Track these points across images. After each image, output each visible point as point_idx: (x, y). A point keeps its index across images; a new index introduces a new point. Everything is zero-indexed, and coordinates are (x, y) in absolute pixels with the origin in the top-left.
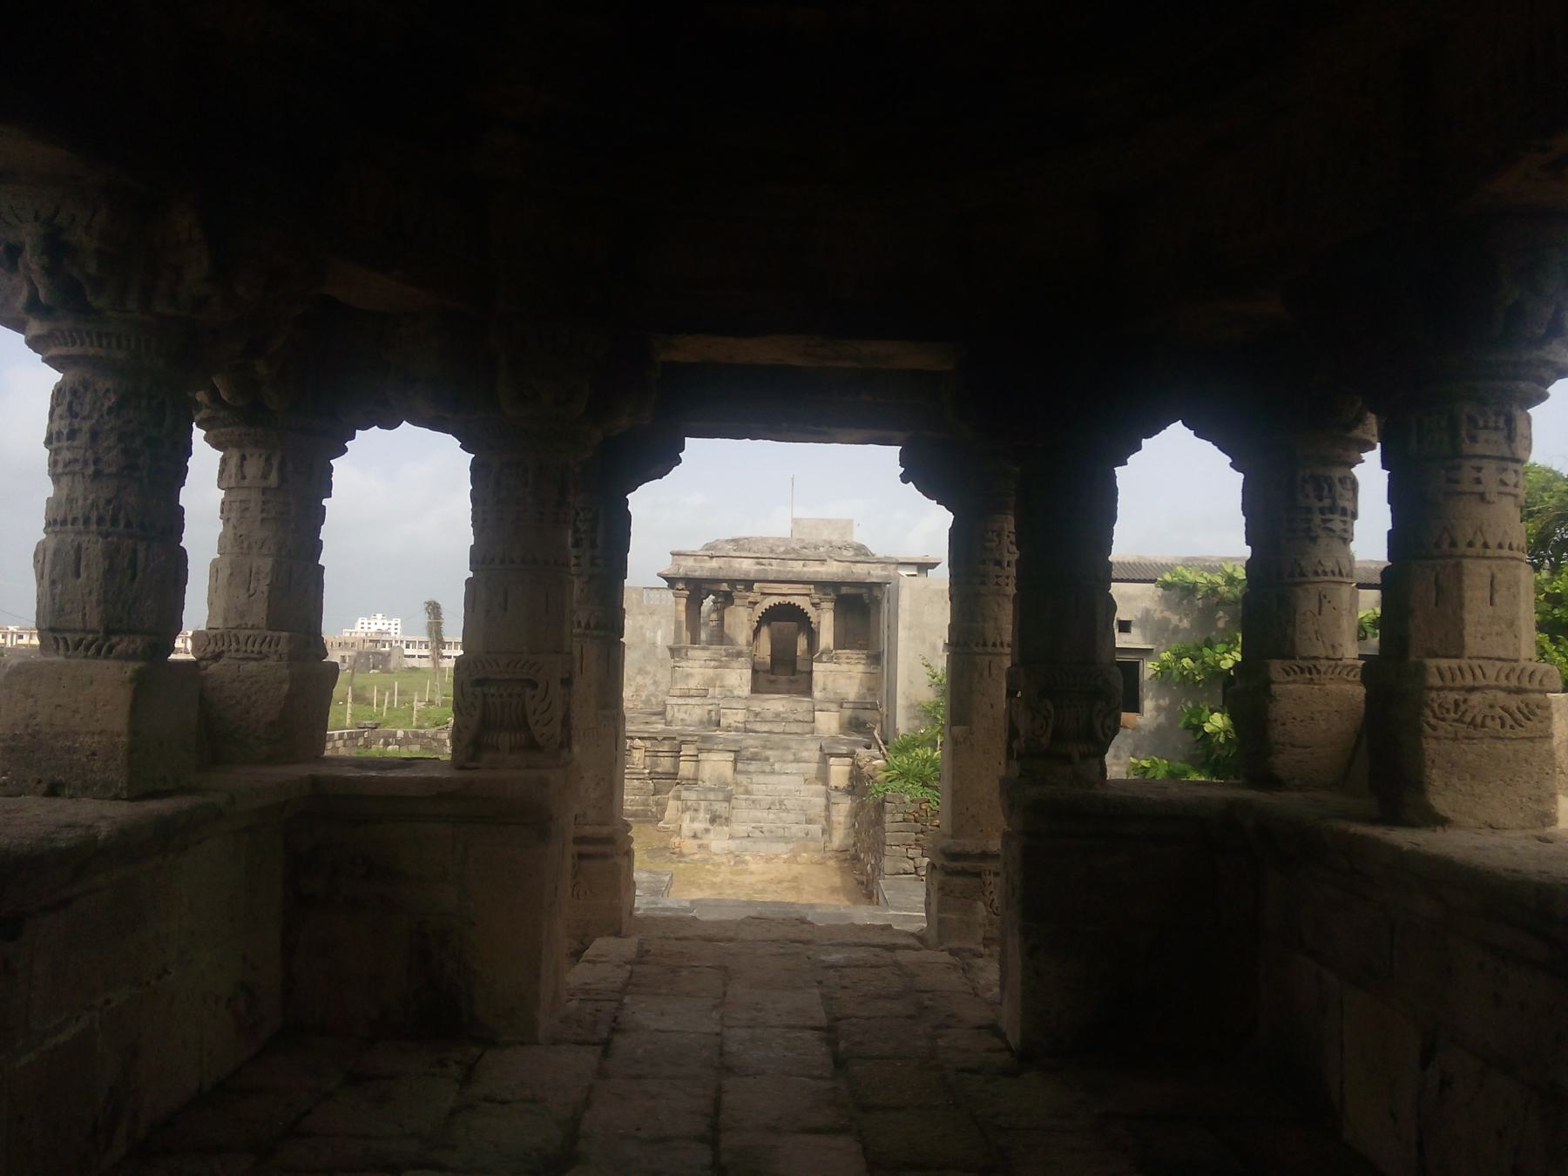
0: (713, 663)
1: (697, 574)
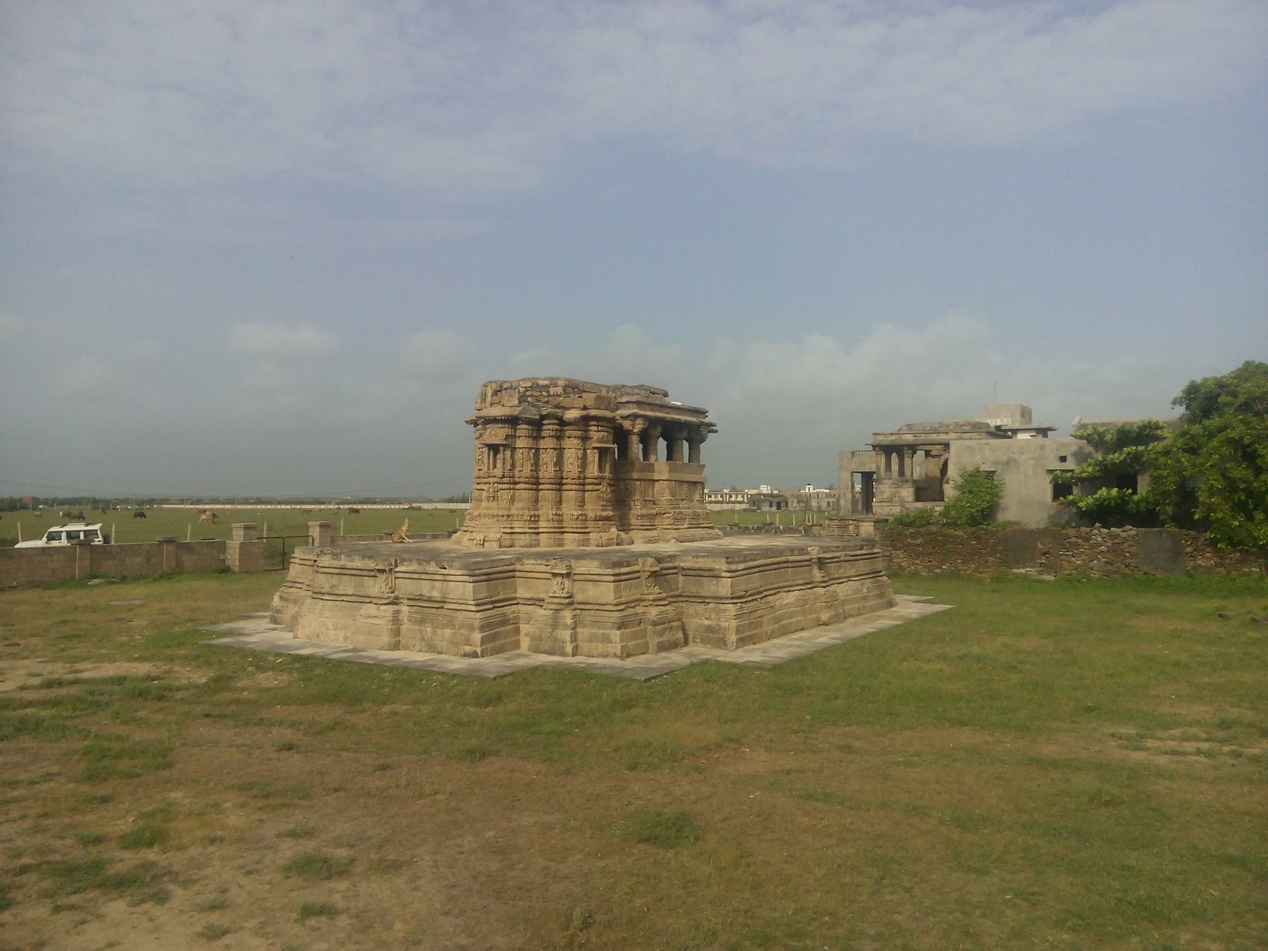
0: (894, 486)
1: (884, 443)
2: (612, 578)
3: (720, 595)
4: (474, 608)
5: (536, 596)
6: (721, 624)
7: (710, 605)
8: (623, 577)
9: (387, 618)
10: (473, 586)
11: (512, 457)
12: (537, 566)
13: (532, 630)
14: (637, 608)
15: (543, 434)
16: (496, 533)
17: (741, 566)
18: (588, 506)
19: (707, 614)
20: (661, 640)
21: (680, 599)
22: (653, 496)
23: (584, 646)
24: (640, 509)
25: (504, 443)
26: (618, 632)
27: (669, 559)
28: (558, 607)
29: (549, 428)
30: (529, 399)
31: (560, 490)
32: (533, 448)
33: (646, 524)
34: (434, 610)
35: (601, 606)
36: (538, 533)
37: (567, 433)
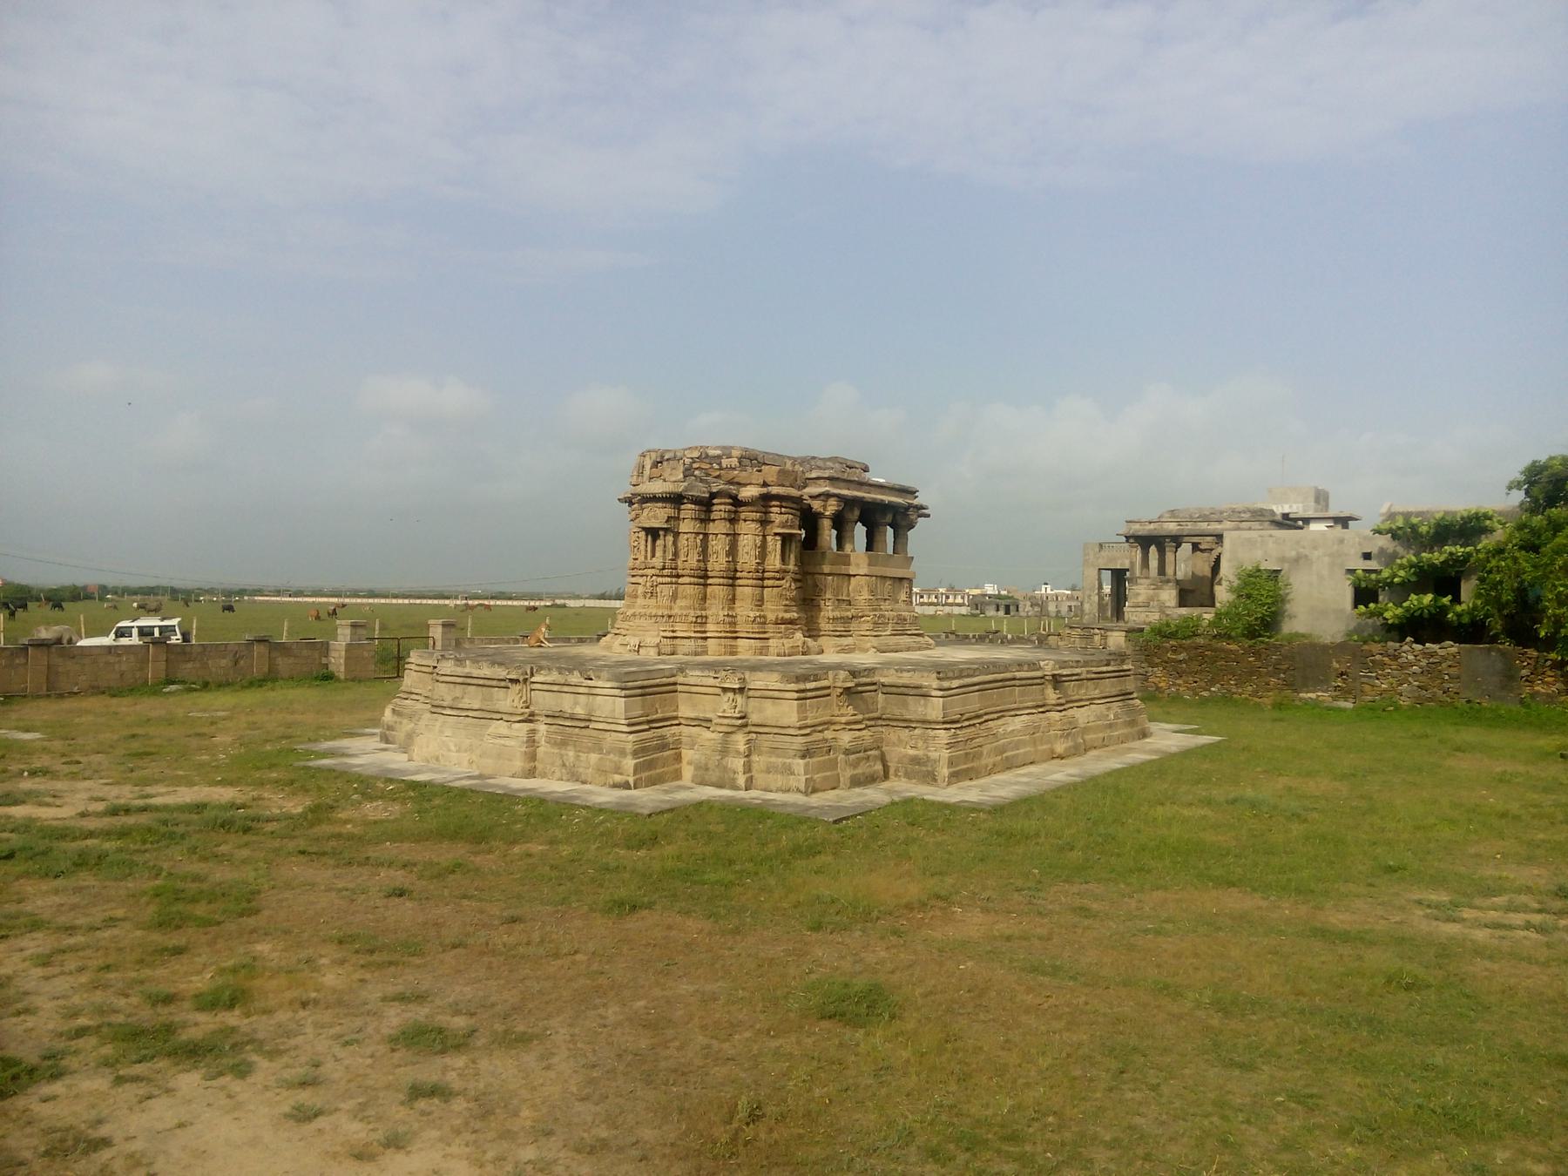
1: (1140, 533)
2: (796, 695)
3: (929, 718)
5: (701, 715)
6: (930, 754)
7: (916, 731)
8: (809, 694)
11: (675, 543)
12: (703, 679)
13: (697, 757)
17: (956, 683)
18: (768, 605)
21: (880, 722)
22: (848, 595)
23: (760, 778)
26: (802, 762)
28: (730, 729)
29: (720, 508)
30: (697, 472)
34: (577, 730)
36: (706, 638)
37: (743, 516)
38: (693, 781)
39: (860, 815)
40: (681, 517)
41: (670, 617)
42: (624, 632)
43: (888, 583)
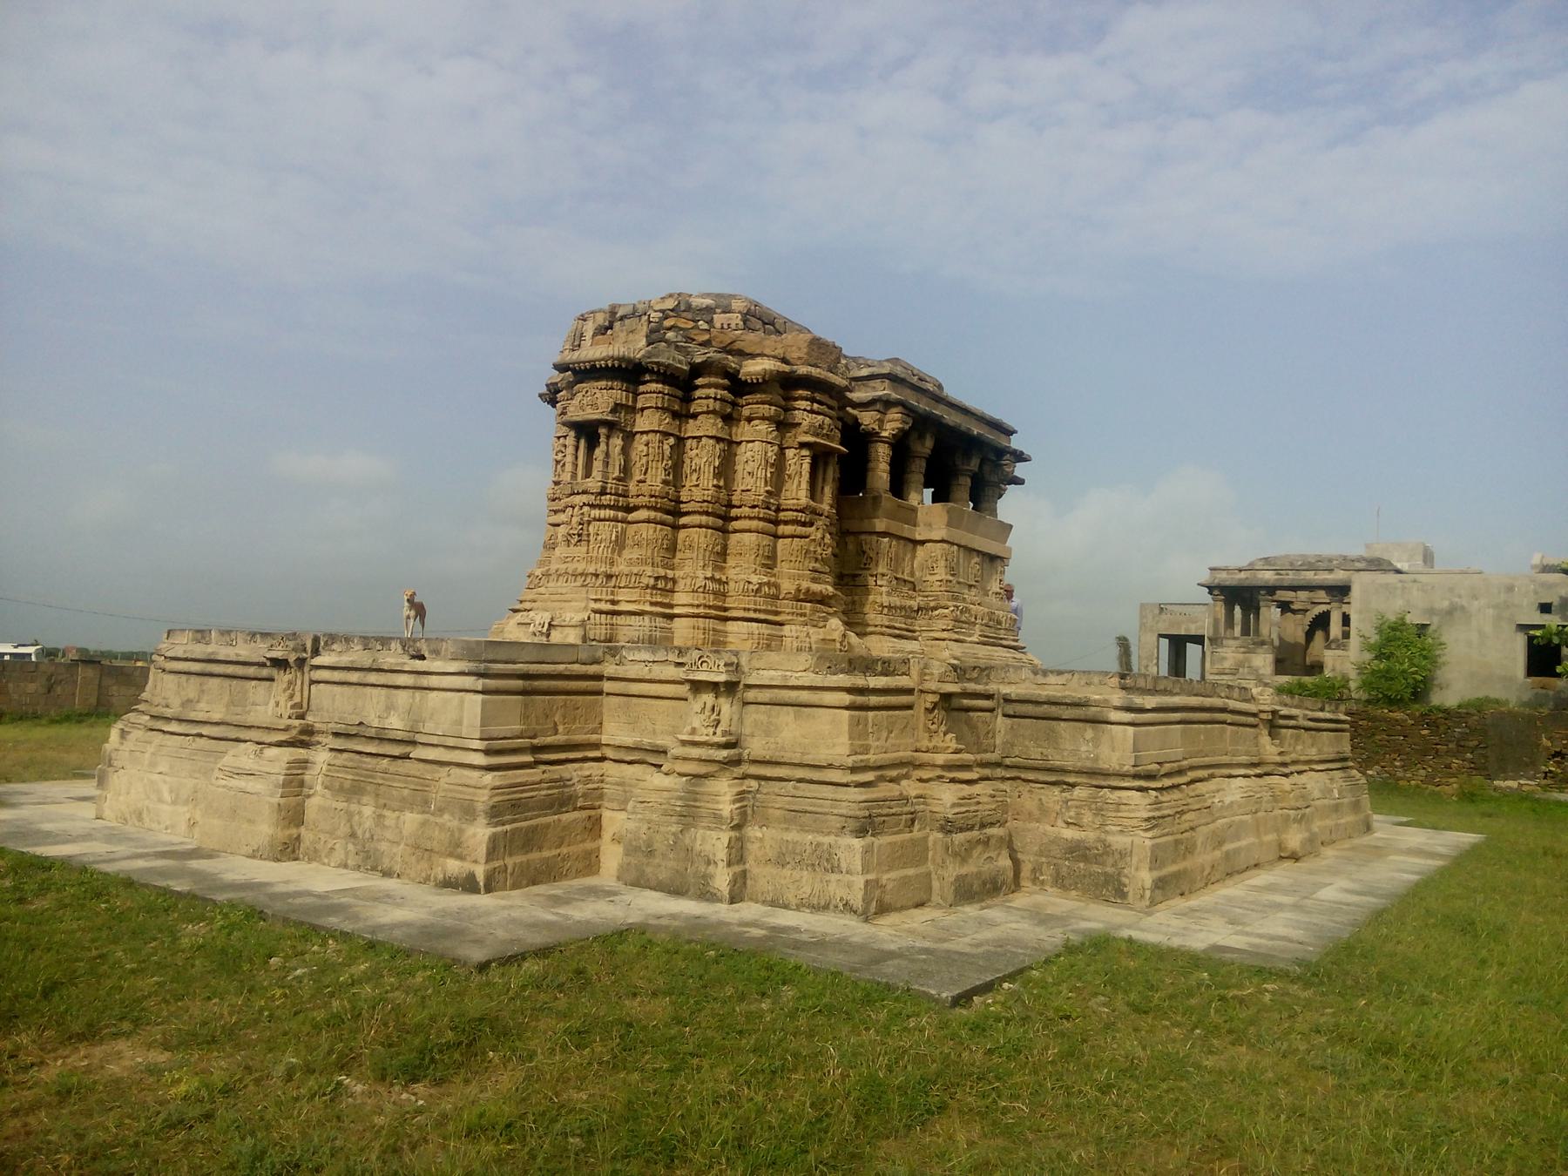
0: (1242, 650)
1: (1227, 583)
2: (847, 699)
3: (1103, 765)
4: (480, 759)
5: (646, 741)
6: (1110, 839)
7: (1077, 792)
8: (874, 700)
9: (273, 777)
10: (484, 703)
11: (625, 451)
12: (655, 667)
13: (631, 825)
14: (904, 783)
15: (694, 408)
16: (578, 611)
17: (1150, 702)
18: (783, 568)
19: (1072, 814)
20: (964, 870)
21: (999, 772)
22: (912, 574)
23: (763, 876)
24: (889, 594)
25: (610, 418)
26: (857, 843)
27: (975, 674)
28: (702, 769)
29: (708, 394)
30: (670, 335)
31: (725, 531)
32: (672, 435)
33: (897, 625)
34: (386, 761)
35: (813, 771)
36: (671, 617)
37: (746, 412)
38: (619, 878)
39: (1010, 977)
40: (639, 405)
41: (609, 577)
42: (527, 605)
43: (976, 559)
